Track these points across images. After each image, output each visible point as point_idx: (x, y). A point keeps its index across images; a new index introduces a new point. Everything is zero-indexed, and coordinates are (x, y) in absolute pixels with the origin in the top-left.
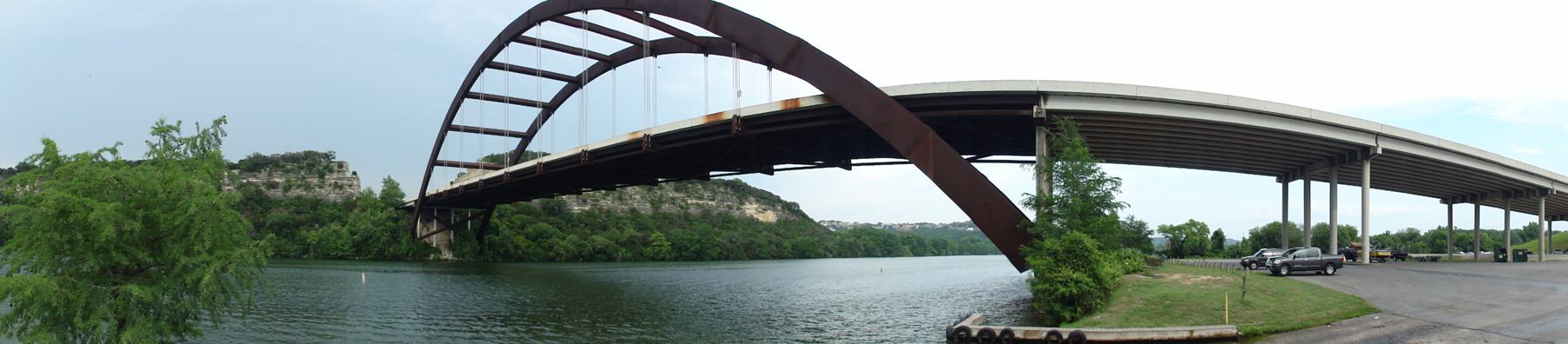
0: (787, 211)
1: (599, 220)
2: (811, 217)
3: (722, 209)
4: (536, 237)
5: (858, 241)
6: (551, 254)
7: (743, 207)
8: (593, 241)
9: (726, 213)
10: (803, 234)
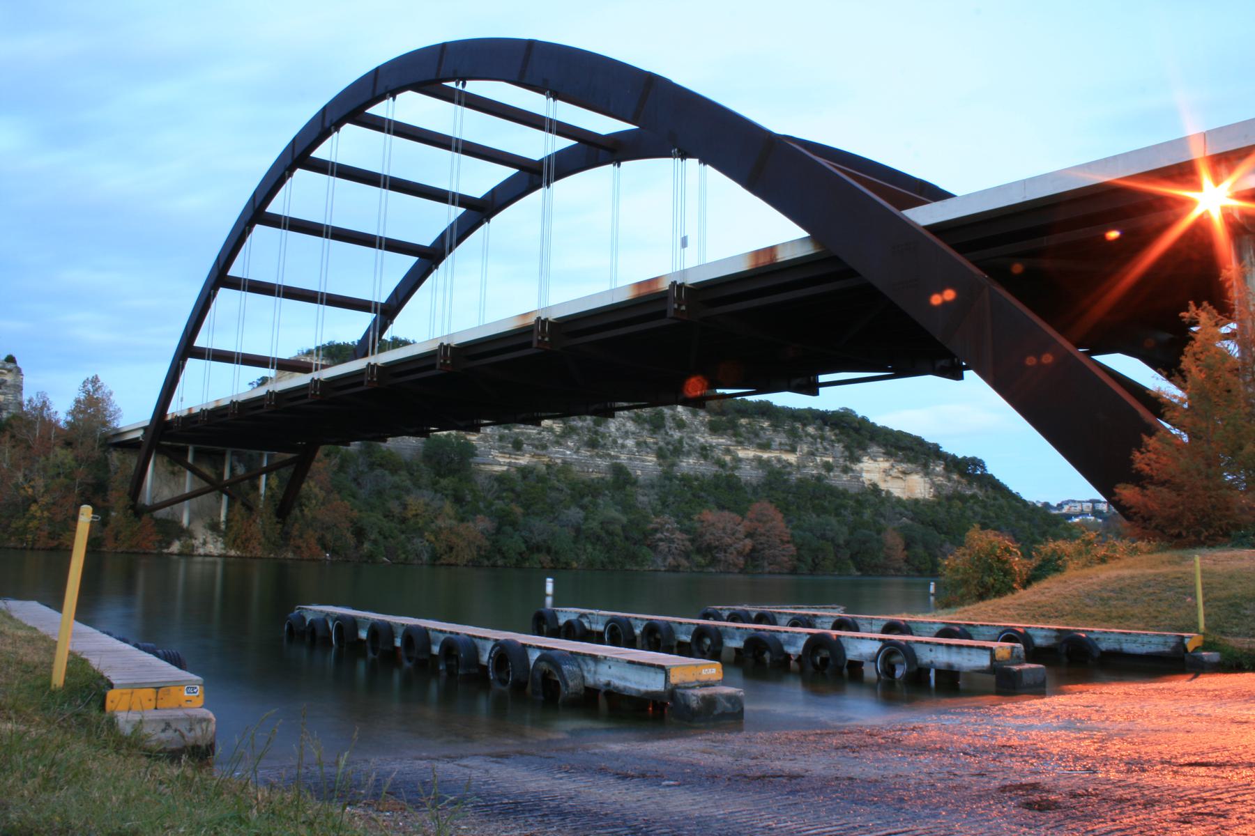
0: (955, 477)
3: (812, 471)
7: (857, 467)
9: (819, 478)
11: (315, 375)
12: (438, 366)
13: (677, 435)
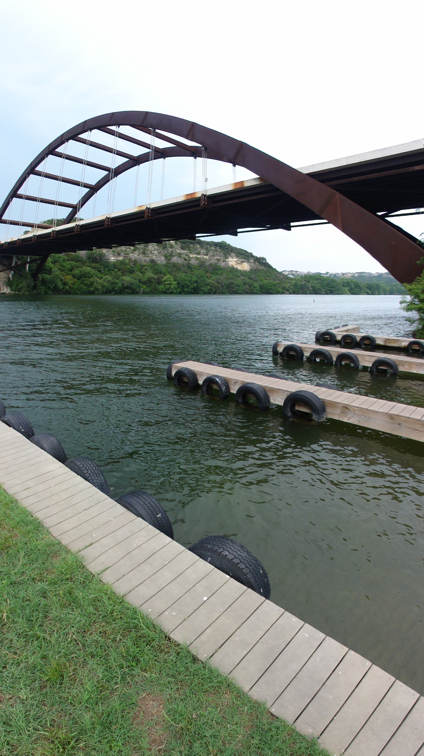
1: (128, 266)
2: (274, 267)
3: (213, 261)
5: (307, 284)
6: (92, 289)
7: (227, 260)
8: (123, 280)
9: (216, 264)
10: (268, 279)
12: (105, 225)
13: (171, 250)
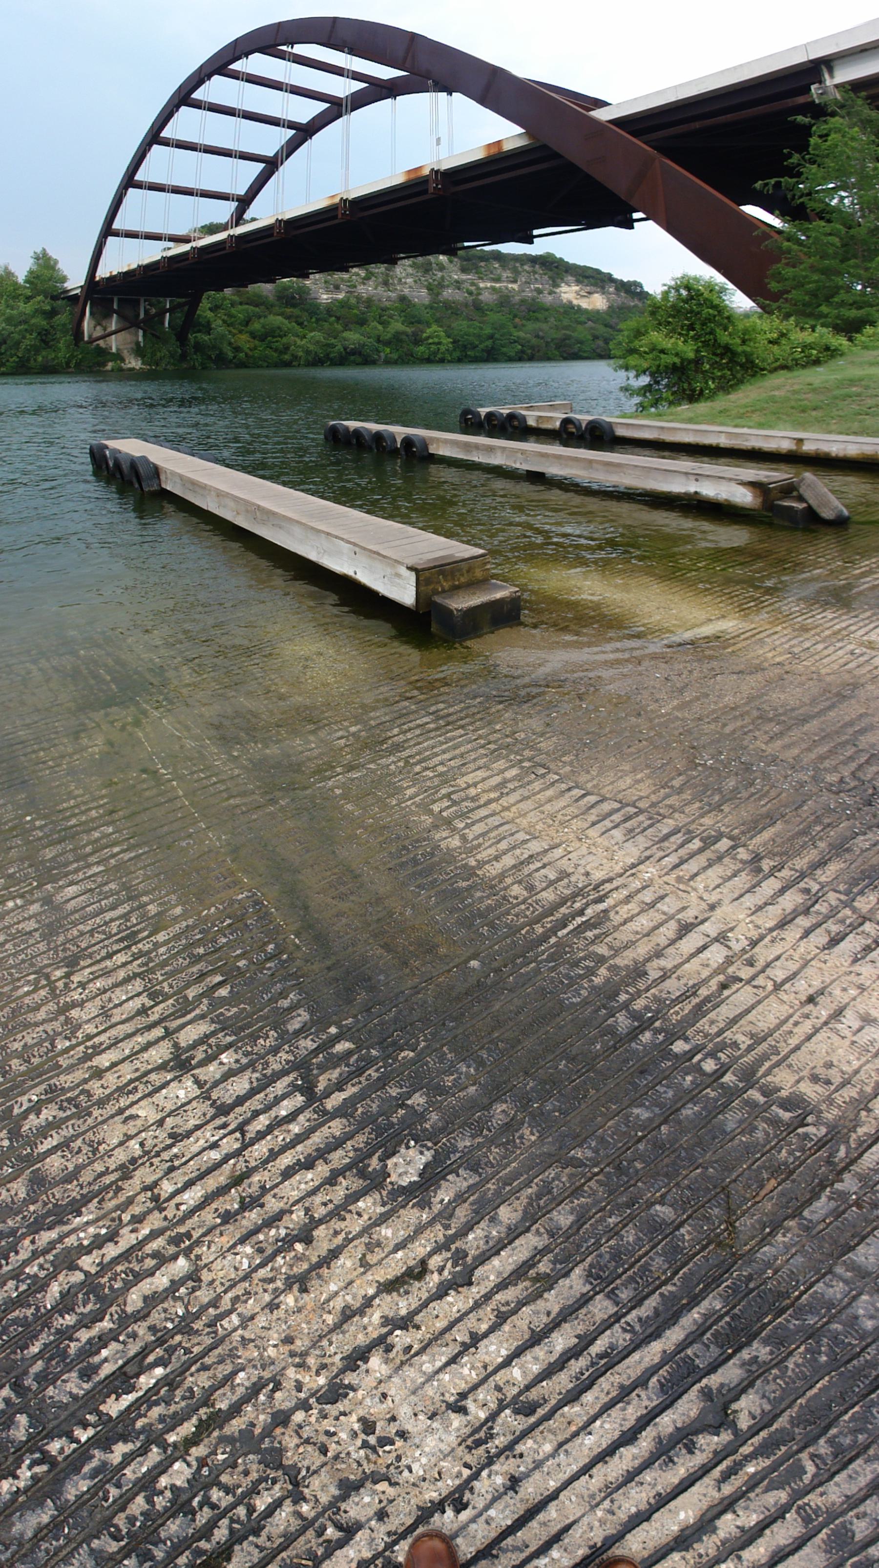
3: (528, 294)
4: (267, 335)
6: (287, 357)
11: (194, 244)
13: (440, 274)
